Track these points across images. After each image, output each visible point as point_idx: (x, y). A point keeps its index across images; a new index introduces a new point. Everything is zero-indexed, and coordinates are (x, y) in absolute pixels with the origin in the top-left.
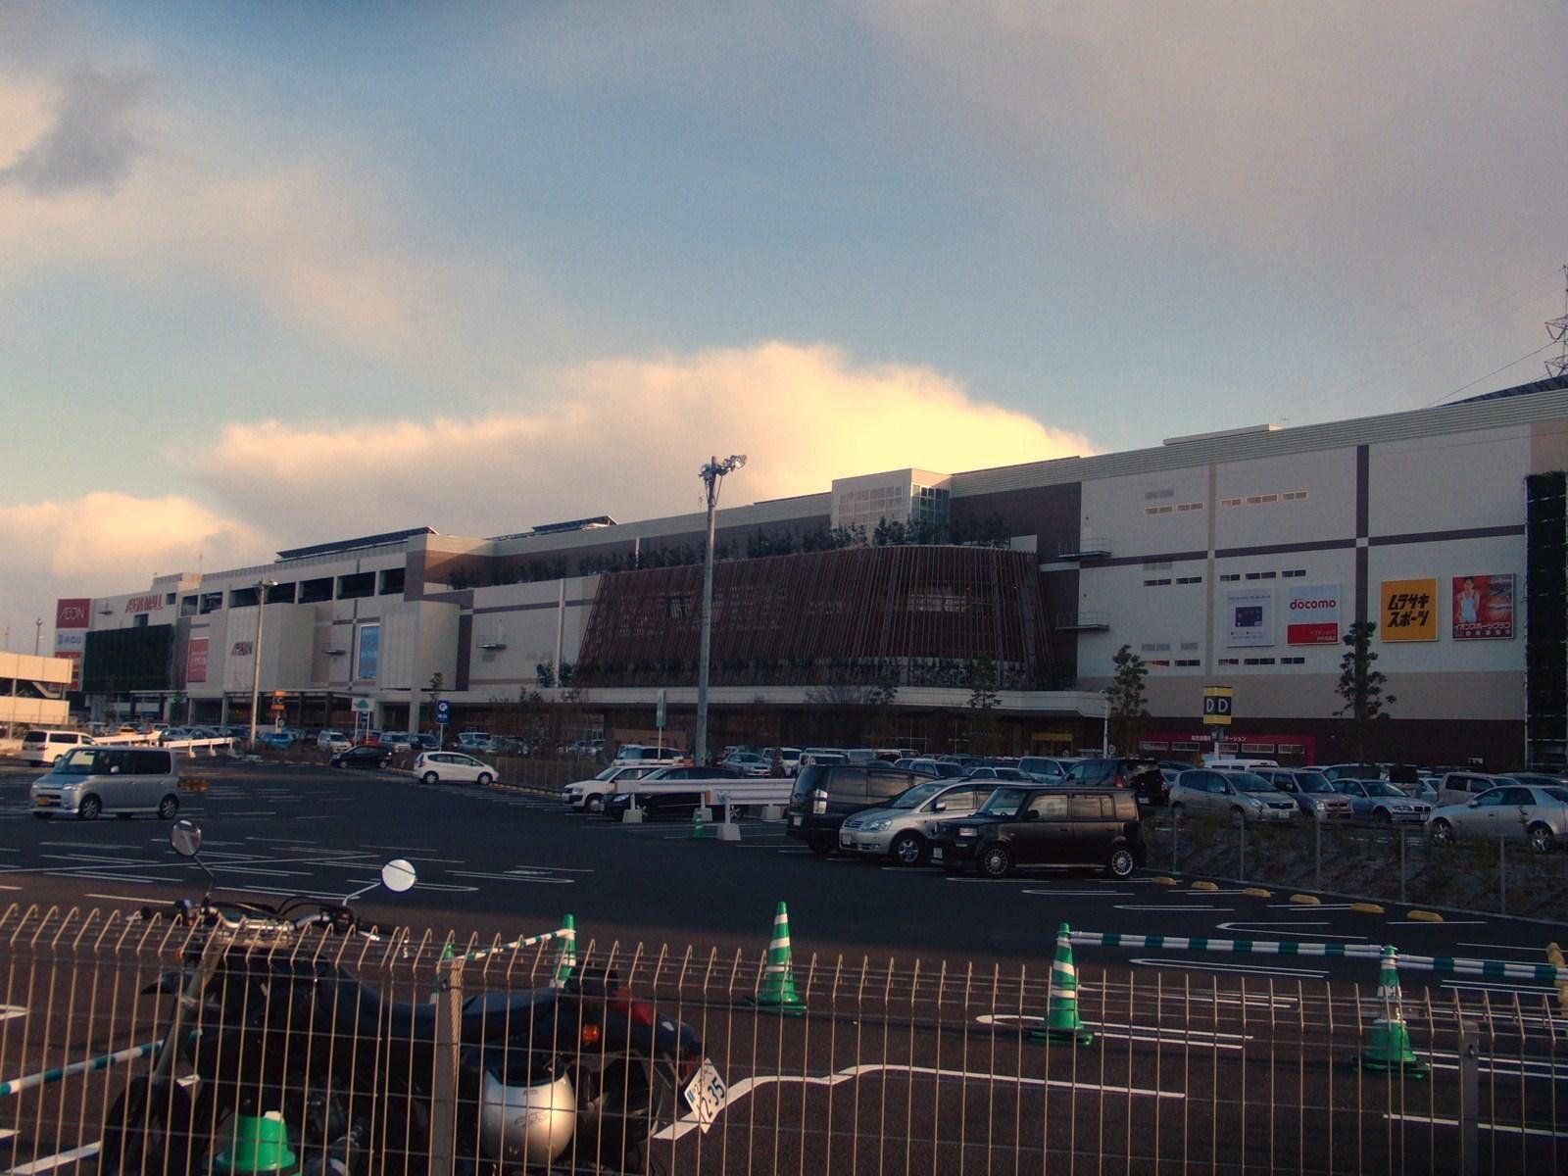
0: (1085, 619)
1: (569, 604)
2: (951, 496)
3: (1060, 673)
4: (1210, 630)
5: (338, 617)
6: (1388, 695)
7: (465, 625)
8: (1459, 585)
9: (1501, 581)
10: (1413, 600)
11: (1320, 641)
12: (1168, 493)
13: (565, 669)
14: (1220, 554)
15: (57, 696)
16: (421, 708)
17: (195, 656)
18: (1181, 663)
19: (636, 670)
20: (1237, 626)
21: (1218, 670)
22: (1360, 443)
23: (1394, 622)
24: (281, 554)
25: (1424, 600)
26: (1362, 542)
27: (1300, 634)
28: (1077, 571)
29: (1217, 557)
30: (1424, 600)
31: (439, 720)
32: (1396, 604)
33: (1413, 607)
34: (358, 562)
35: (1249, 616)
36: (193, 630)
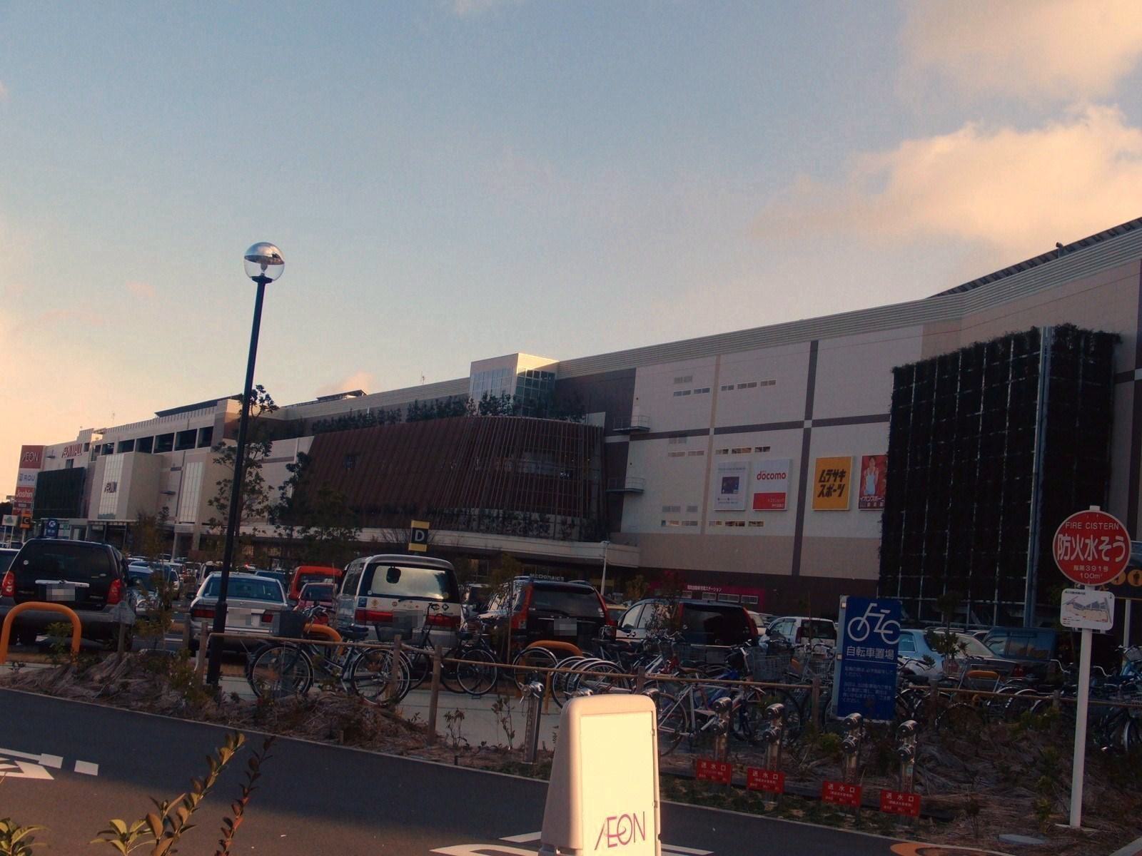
0: (629, 485)
2: (556, 378)
5: (174, 465)
10: (836, 474)
11: (774, 508)
12: (689, 379)
14: (719, 431)
16: (201, 539)
18: (687, 523)
20: (722, 493)
21: (710, 530)
22: (813, 339)
24: (157, 413)
26: (808, 424)
28: (627, 444)
29: (709, 429)
30: (842, 475)
32: (825, 478)
33: (835, 481)
35: (730, 485)
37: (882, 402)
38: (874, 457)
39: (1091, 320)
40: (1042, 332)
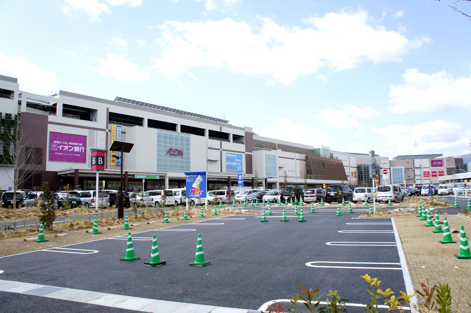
1: (297, 159)
6: (130, 225)
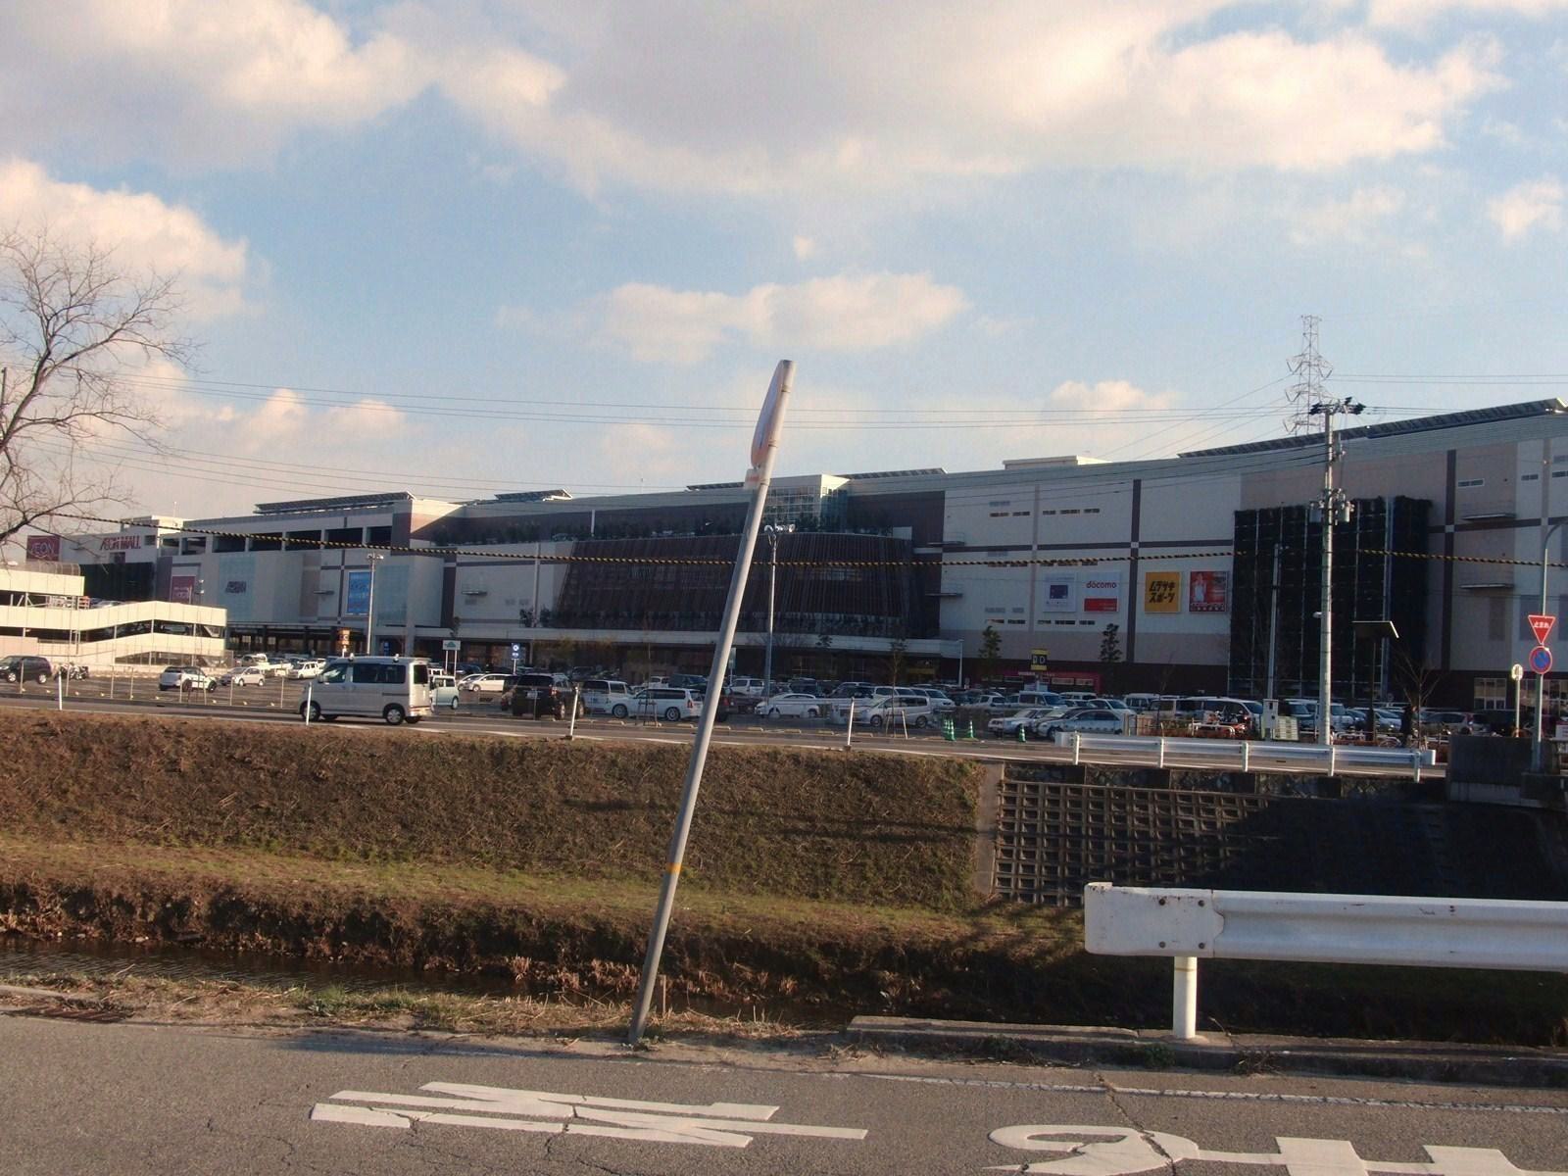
2: (849, 495)
3: (928, 627)
4: (1032, 597)
7: (449, 578)
8: (1194, 576)
9: (1219, 576)
10: (1165, 585)
12: (1007, 503)
13: (545, 614)
14: (1041, 547)
15: (217, 635)
17: (177, 591)
19: (608, 616)
21: (1038, 628)
23: (1153, 599)
24: (260, 506)
25: (1172, 585)
27: (1093, 605)
30: (1172, 585)
31: (513, 657)
34: (346, 519)
35: (1059, 592)
36: (174, 569)
37: (1229, 533)
38: (1203, 573)
39: (1416, 492)
40: (1387, 501)
